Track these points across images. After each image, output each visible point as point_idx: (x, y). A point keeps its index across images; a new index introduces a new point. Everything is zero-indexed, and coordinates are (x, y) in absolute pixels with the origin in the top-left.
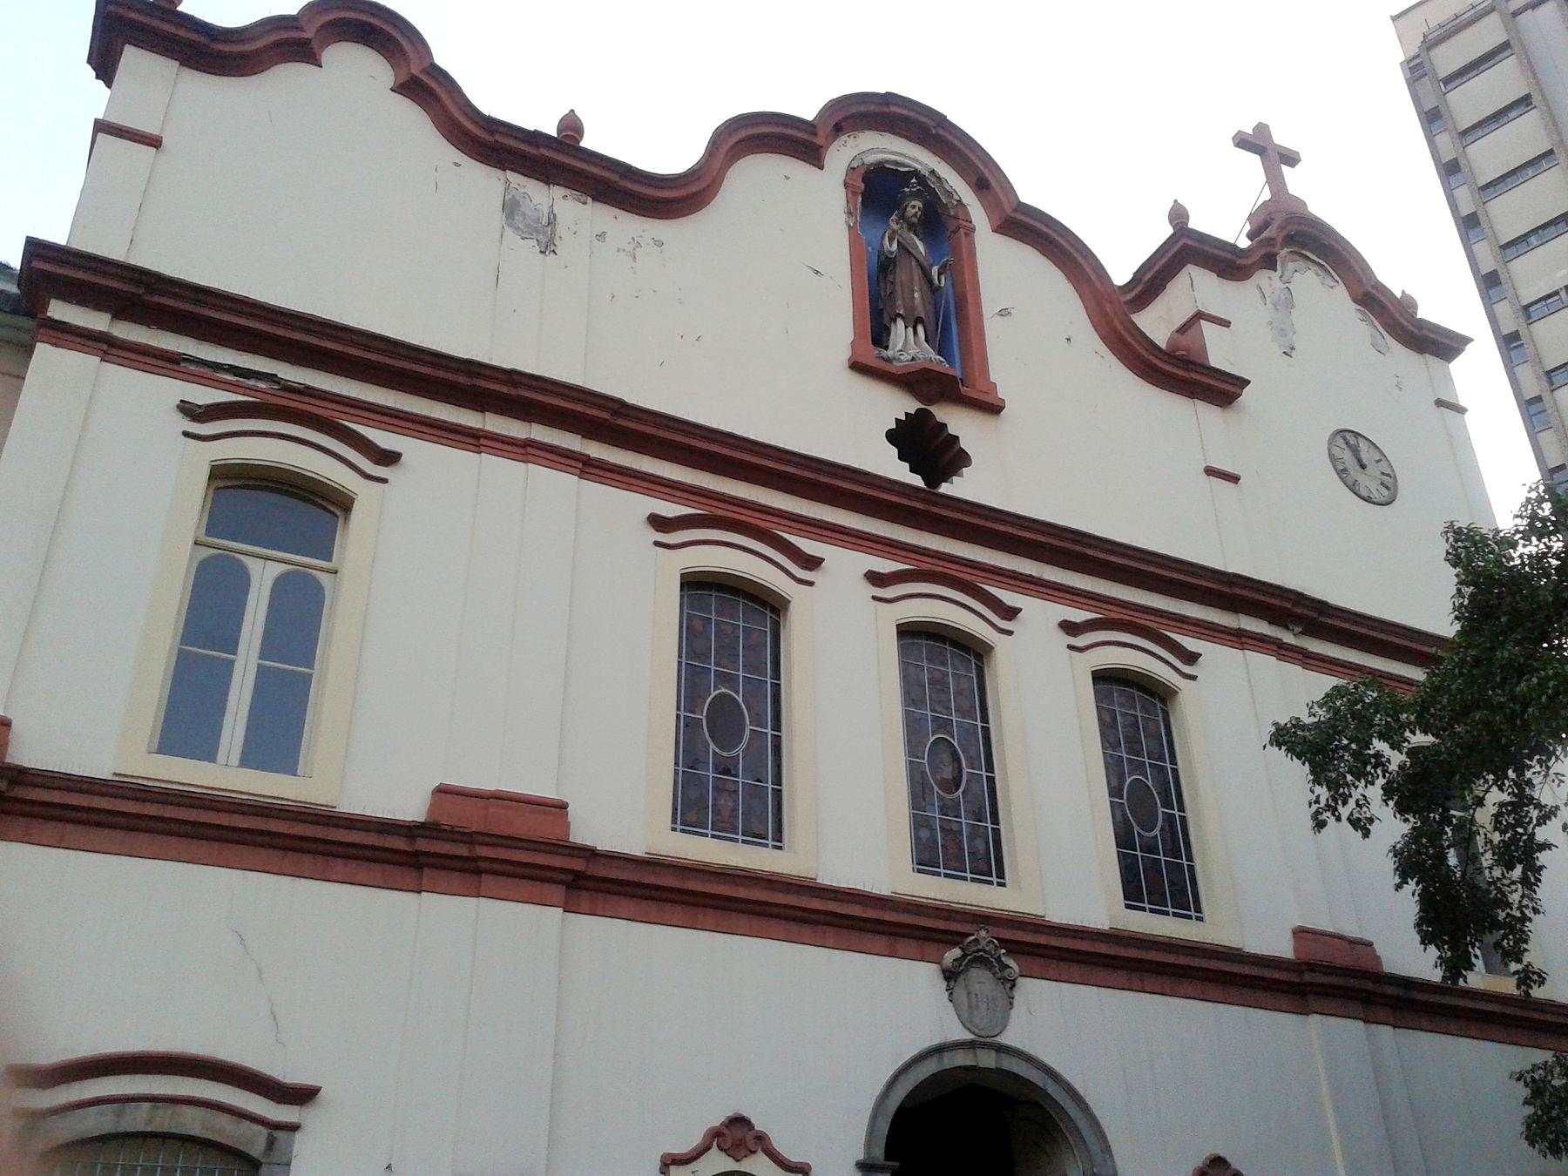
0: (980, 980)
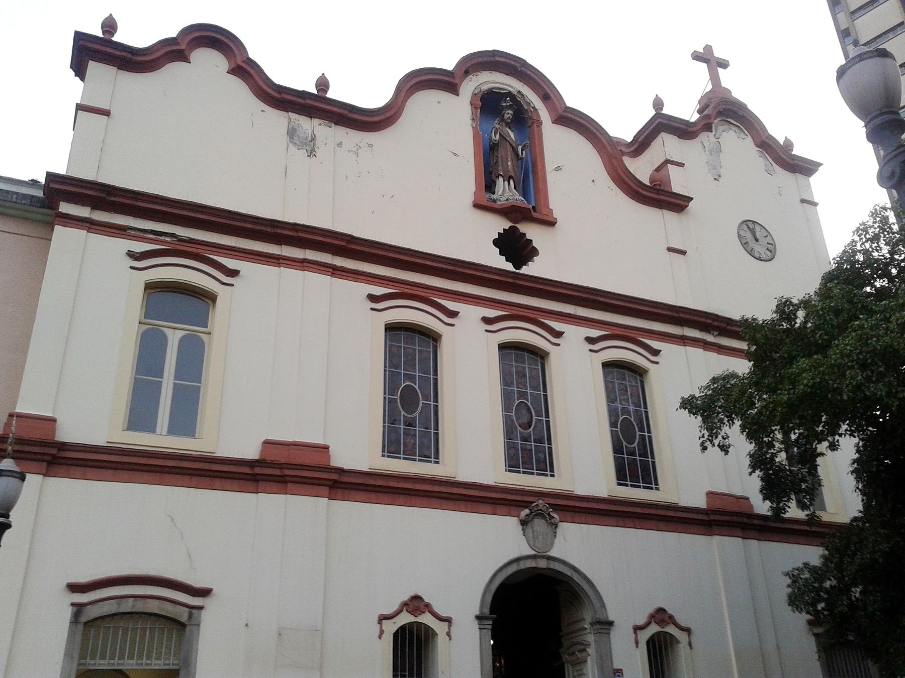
0: (539, 525)
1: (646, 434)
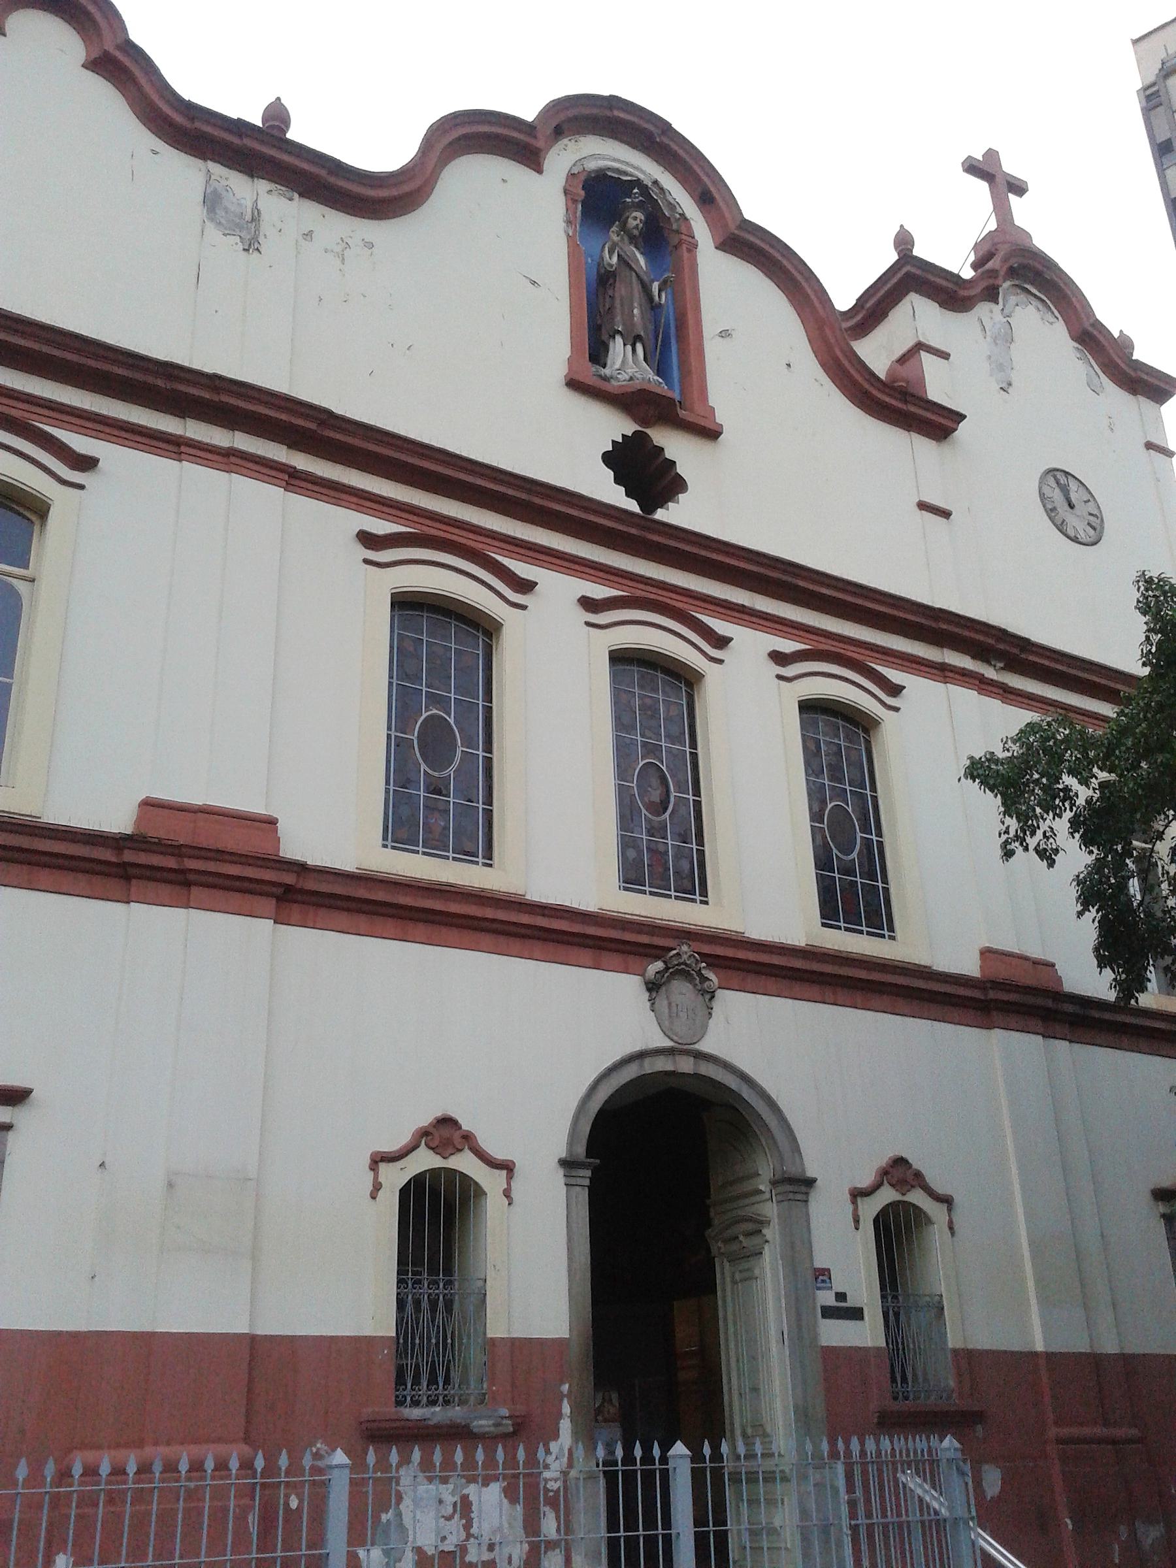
0: (681, 991)
1: (875, 838)
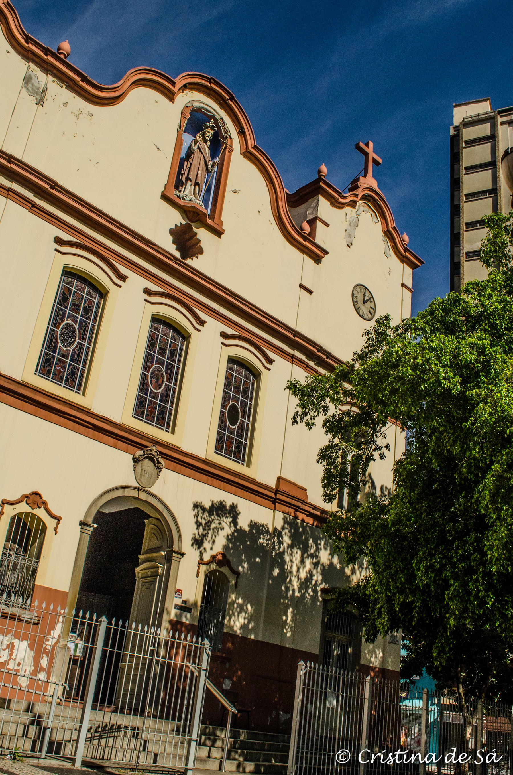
1: (246, 421)
